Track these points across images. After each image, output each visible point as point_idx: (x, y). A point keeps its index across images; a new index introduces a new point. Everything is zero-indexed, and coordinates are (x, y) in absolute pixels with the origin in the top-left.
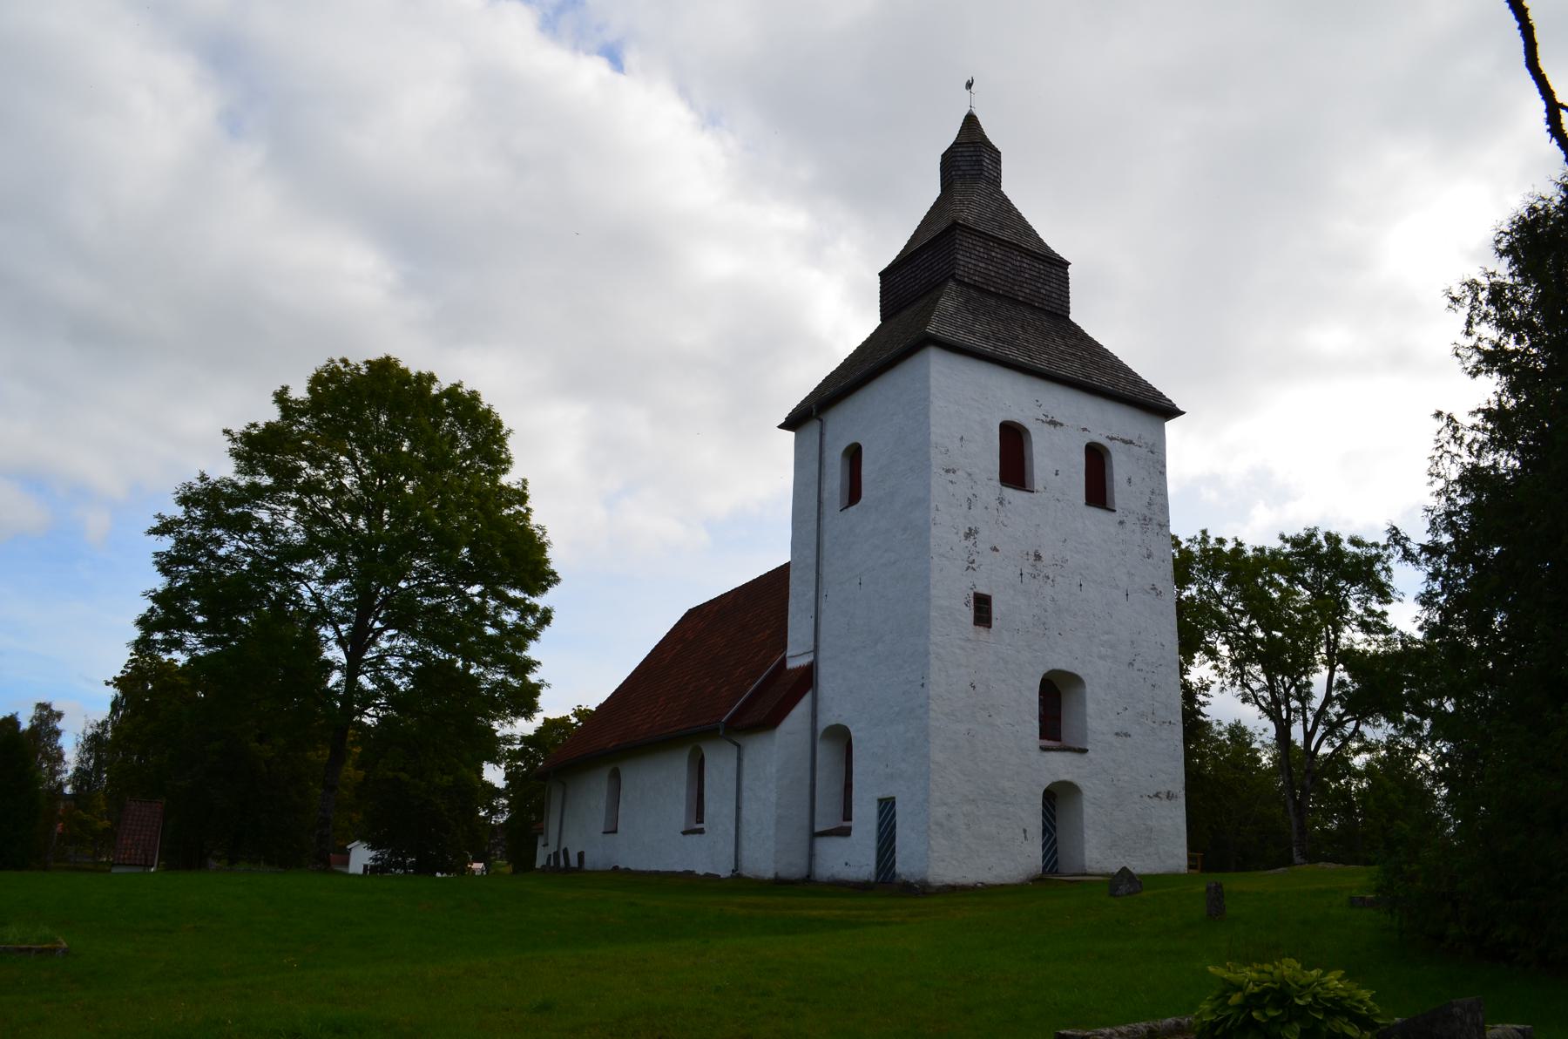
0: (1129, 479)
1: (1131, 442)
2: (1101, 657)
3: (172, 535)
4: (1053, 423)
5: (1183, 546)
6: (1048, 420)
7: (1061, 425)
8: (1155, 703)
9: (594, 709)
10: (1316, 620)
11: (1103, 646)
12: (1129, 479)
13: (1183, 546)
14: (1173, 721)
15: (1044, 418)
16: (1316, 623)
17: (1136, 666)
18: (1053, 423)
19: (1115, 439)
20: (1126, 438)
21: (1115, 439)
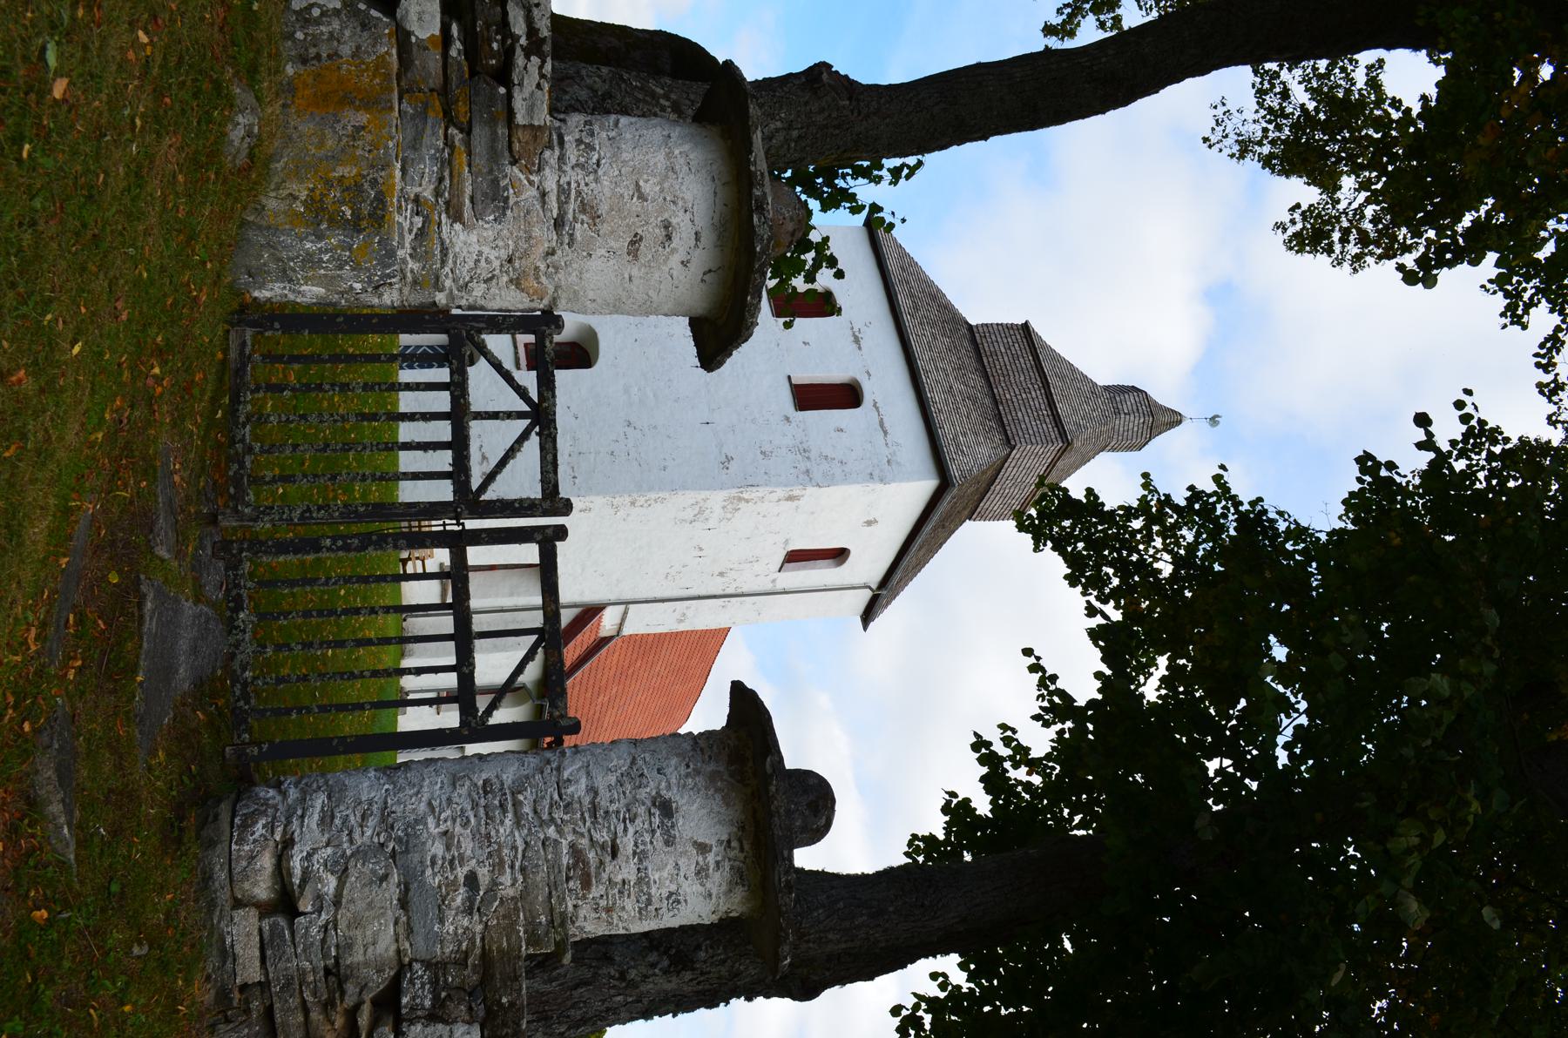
0: (842, 430)
1: (885, 433)
2: (627, 390)
3: (60, 228)
4: (857, 340)
5: (1353, 88)
6: (857, 334)
7: (860, 348)
8: (593, 455)
9: (1424, 52)
10: (1216, 803)
11: (639, 389)
12: (842, 430)
13: (1353, 88)
14: (577, 481)
15: (856, 329)
16: (1210, 802)
17: (629, 431)
18: (857, 340)
19: (877, 409)
20: (886, 425)
21: (877, 409)
